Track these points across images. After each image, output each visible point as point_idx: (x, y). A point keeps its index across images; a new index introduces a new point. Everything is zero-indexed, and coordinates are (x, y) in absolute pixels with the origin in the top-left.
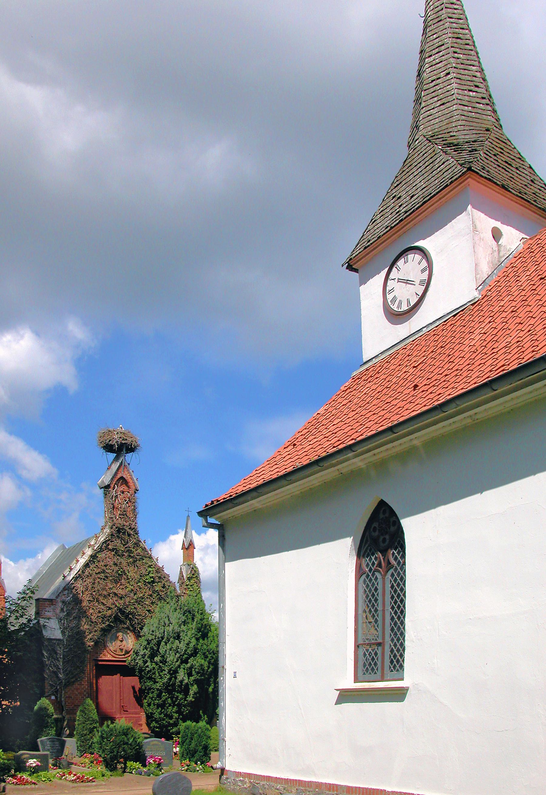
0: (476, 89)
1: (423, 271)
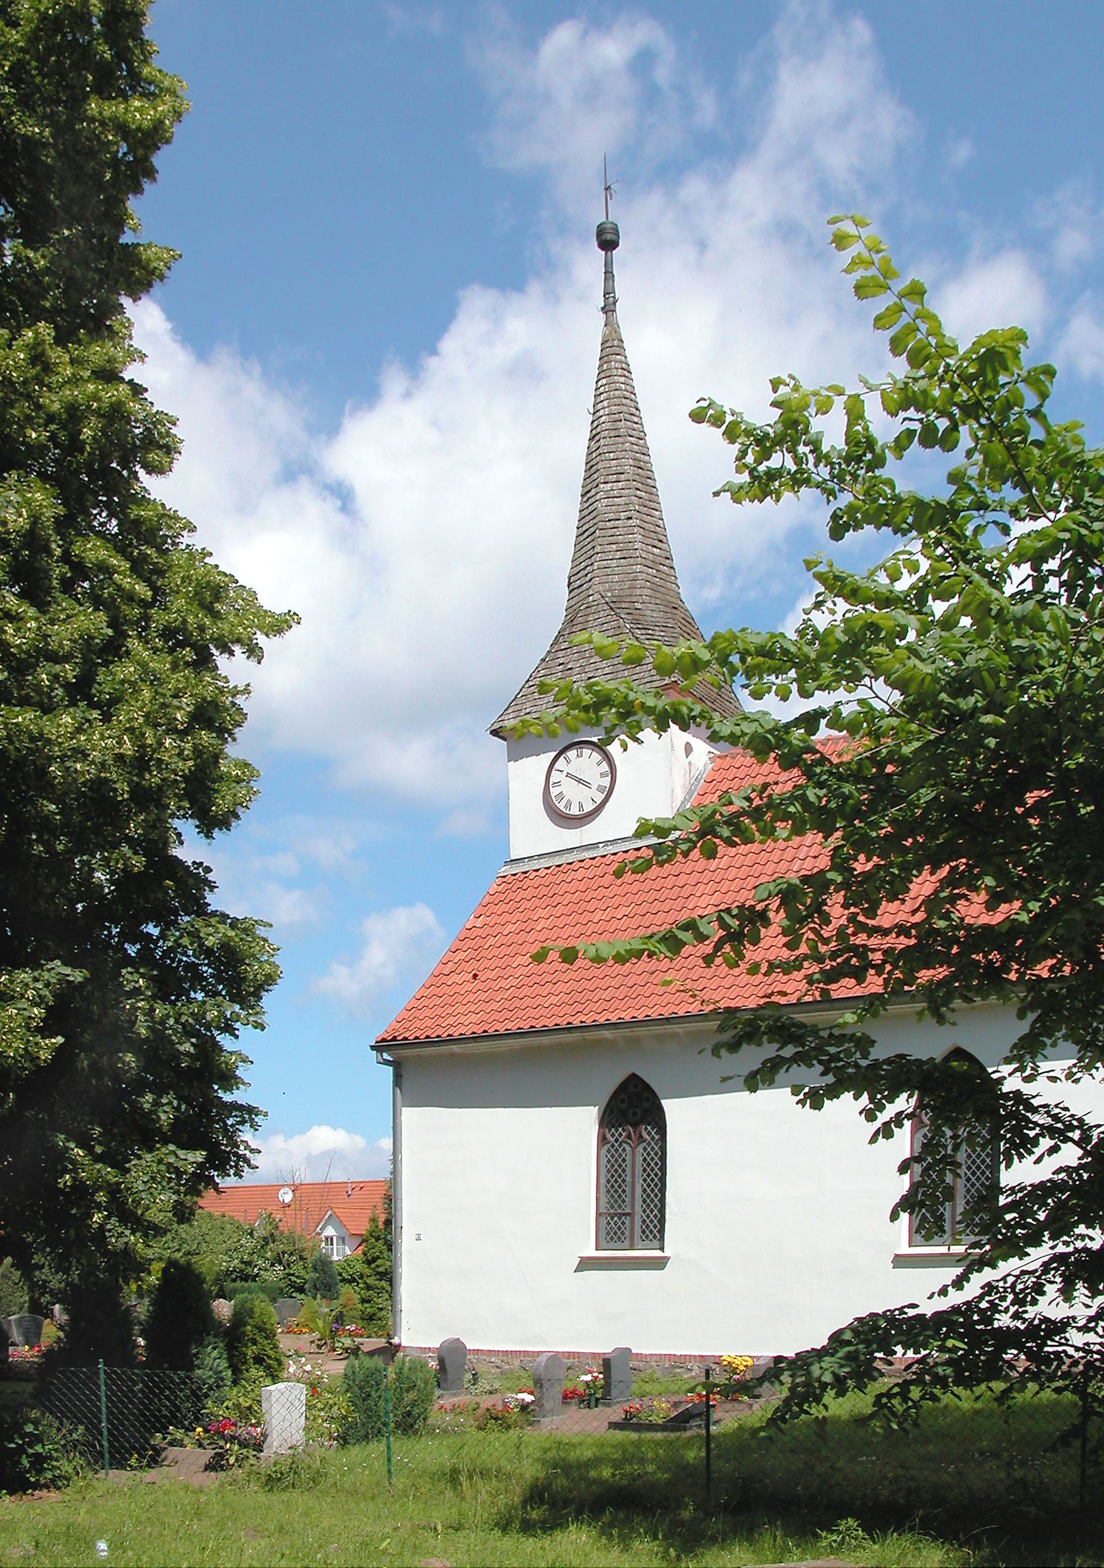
0: (659, 545)
1: (602, 775)
